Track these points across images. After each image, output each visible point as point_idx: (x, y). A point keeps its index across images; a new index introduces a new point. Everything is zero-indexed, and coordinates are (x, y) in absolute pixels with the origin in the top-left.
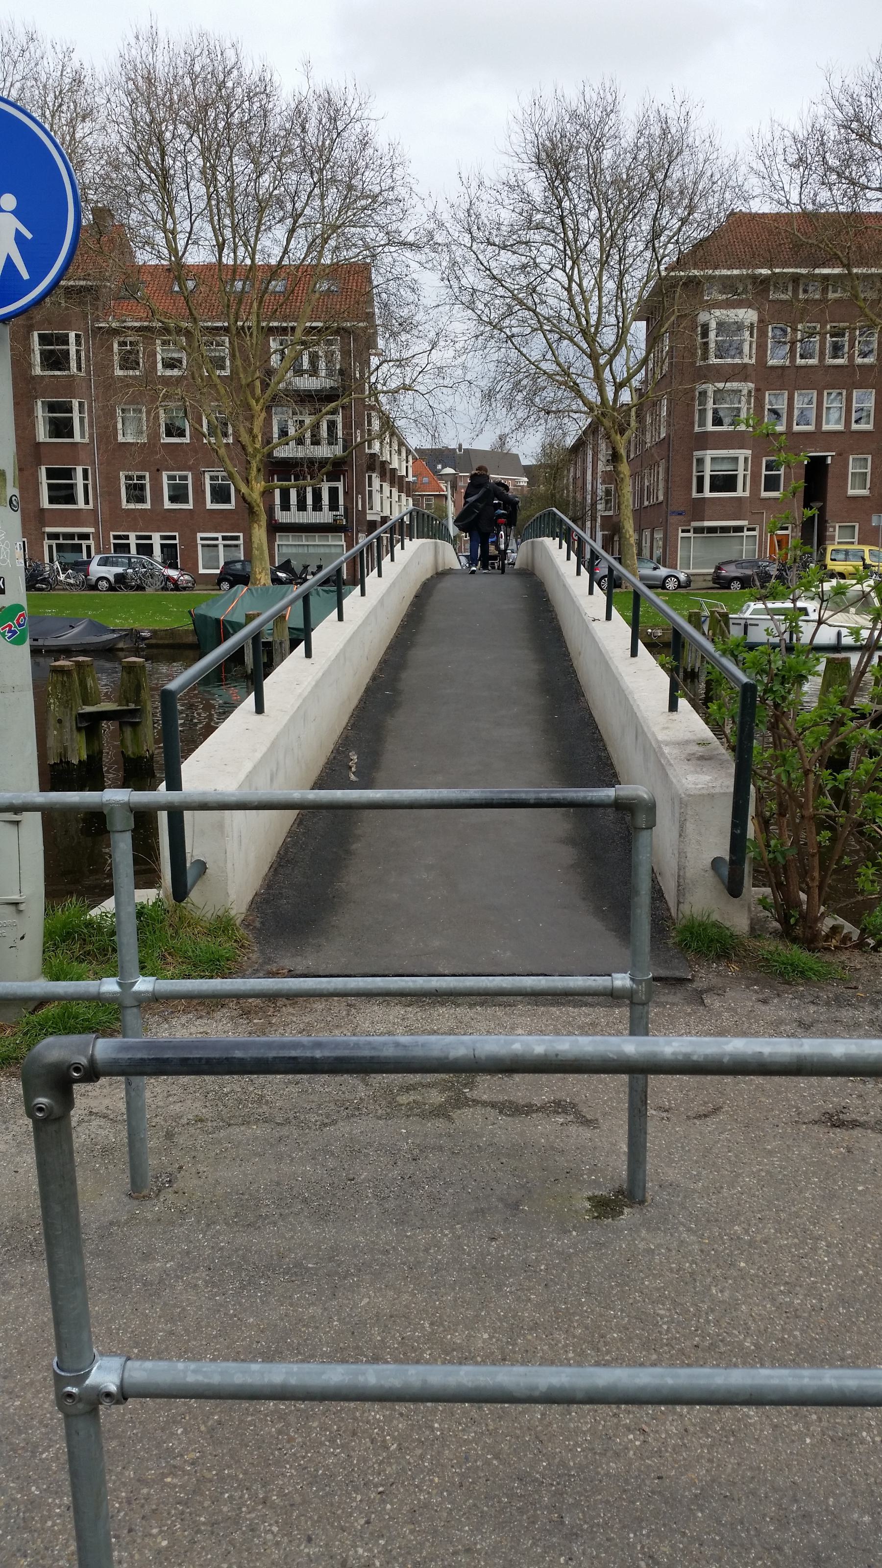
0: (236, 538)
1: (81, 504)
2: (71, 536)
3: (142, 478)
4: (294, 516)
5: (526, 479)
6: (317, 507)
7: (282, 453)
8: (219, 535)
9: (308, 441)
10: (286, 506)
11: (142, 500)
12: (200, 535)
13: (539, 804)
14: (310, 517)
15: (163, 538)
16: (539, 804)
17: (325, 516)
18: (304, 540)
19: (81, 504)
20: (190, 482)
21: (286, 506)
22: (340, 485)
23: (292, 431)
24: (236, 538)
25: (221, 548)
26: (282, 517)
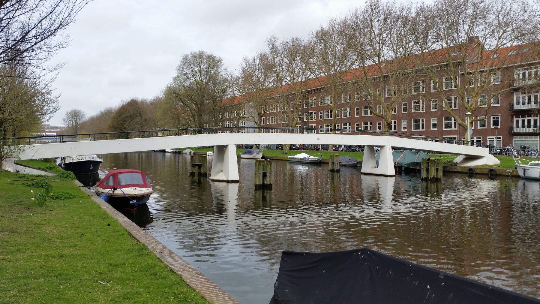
0: (500, 138)
1: (453, 128)
2: (450, 138)
3: (498, 118)
4: (521, 130)
5: (237, 94)
6: (529, 126)
7: (516, 107)
8: (494, 137)
9: (526, 103)
10: (518, 127)
11: (484, 126)
12: (488, 137)
13: (189, 256)
14: (526, 130)
15: (477, 138)
16: (189, 256)
17: (530, 130)
18: (523, 138)
19: (453, 128)
20: (499, 119)
21: (518, 127)
22: (538, 118)
23: (521, 100)
24: (500, 138)
25: (495, 142)
26: (516, 130)
